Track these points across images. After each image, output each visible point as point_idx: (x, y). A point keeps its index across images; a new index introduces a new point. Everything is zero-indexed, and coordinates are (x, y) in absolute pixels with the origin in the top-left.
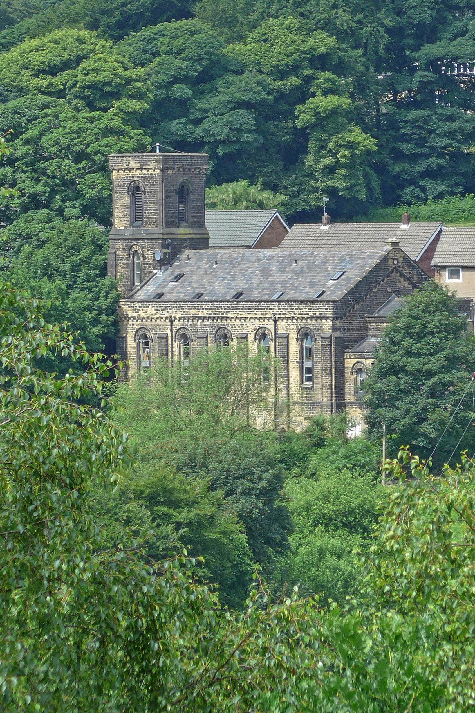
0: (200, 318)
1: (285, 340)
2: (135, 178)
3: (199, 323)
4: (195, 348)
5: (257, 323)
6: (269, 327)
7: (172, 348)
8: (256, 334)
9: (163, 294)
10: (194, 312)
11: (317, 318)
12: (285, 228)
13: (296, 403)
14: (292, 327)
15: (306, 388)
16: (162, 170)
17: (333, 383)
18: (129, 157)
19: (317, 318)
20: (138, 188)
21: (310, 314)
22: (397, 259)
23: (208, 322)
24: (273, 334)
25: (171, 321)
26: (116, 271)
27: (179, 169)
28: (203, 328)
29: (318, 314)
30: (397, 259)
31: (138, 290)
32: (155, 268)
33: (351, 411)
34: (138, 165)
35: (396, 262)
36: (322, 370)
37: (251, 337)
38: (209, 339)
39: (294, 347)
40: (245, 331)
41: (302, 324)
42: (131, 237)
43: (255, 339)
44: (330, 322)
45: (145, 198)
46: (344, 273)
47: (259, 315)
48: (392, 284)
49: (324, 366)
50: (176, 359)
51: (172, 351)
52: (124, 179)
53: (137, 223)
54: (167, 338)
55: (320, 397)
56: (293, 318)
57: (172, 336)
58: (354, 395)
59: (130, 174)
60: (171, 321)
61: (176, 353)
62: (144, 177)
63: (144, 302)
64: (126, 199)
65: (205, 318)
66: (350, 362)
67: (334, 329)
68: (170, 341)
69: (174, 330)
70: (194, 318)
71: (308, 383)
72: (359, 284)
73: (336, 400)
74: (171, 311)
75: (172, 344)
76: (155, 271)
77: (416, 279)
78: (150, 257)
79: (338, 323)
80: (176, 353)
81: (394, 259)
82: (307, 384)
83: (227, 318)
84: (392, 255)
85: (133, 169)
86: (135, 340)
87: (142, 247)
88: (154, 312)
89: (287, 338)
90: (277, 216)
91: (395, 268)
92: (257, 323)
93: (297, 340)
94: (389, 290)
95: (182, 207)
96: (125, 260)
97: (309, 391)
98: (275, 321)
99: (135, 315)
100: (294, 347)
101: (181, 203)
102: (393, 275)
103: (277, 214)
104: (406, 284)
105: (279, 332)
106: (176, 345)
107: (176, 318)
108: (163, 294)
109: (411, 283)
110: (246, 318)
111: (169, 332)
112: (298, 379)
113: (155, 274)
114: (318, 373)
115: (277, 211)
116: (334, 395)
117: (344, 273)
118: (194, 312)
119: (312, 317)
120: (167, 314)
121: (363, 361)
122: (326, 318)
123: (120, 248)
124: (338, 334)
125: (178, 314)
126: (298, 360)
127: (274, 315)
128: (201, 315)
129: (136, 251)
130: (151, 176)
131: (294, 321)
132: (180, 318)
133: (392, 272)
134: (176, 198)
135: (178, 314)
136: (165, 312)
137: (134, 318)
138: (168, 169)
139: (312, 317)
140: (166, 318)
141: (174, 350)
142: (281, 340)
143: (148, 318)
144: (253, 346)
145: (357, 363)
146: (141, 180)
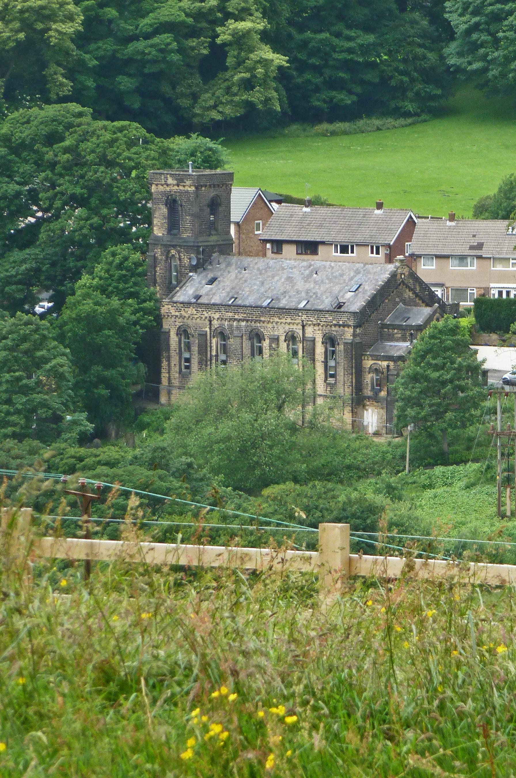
0: (235, 319)
1: (312, 343)
2: (173, 193)
3: (235, 323)
4: (231, 345)
5: (287, 327)
6: (298, 331)
7: (211, 343)
8: (286, 336)
9: (201, 296)
10: (230, 314)
11: (340, 326)
12: (266, 203)
13: (321, 395)
14: (318, 332)
15: (330, 384)
16: (197, 188)
17: (354, 381)
18: (167, 174)
19: (340, 326)
20: (175, 201)
21: (334, 322)
22: (404, 274)
23: (243, 324)
24: (301, 336)
25: (210, 321)
26: (156, 272)
27: (210, 186)
28: (238, 328)
29: (341, 323)
30: (404, 274)
31: (178, 291)
32: (190, 272)
33: (368, 403)
34: (175, 182)
35: (403, 277)
36: (344, 369)
37: (282, 338)
38: (244, 337)
39: (320, 349)
40: (276, 333)
41: (327, 330)
42: (169, 243)
43: (285, 341)
44: (351, 330)
45: (182, 209)
46: (360, 285)
47: (289, 320)
48: (400, 295)
49: (346, 366)
50: (214, 353)
51: (211, 347)
52: (164, 193)
53: (175, 231)
54: (206, 335)
55: (342, 391)
56: (319, 324)
57: (210, 334)
58: (371, 391)
59: (168, 189)
60: (210, 321)
61: (214, 348)
62: (181, 193)
63: (186, 303)
64: (164, 210)
65: (240, 320)
66: (368, 363)
67: (354, 335)
68: (208, 337)
69: (213, 328)
70: (231, 319)
71: (331, 379)
72: (374, 298)
73: (356, 395)
74: (210, 313)
75: (211, 340)
76: (191, 274)
77: (418, 289)
78: (186, 261)
79: (358, 330)
80: (214, 348)
81: (401, 274)
82: (331, 380)
83: (261, 321)
84: (399, 271)
85: (170, 185)
86: (177, 335)
87: (179, 252)
88: (195, 312)
89: (313, 341)
90: (260, 195)
91: (403, 281)
92: (287, 327)
93: (323, 343)
94: (397, 300)
95: (212, 218)
96: (163, 262)
97: (332, 386)
98: (303, 326)
99: (177, 314)
100: (320, 349)
101: (212, 214)
102: (400, 287)
103: (260, 191)
104: (411, 294)
105: (307, 335)
106: (214, 341)
107: (214, 319)
108: (201, 296)
109: (414, 293)
110: (277, 322)
111: (208, 329)
112: (323, 376)
113: (191, 276)
114: (341, 372)
115: (260, 189)
116: (354, 391)
117: (360, 285)
118: (230, 314)
119: (335, 325)
120: (206, 315)
121: (380, 362)
122: (349, 326)
123: (158, 252)
124: (358, 340)
125: (217, 316)
126: (323, 360)
127: (303, 321)
128: (236, 317)
129: (173, 255)
130: (187, 192)
131: (320, 327)
132: (218, 319)
133: (400, 285)
134: (208, 210)
135: (217, 316)
136: (204, 313)
137: (177, 316)
138: (202, 186)
139: (335, 325)
140: (206, 318)
141: (212, 345)
142: (308, 343)
143: (189, 317)
144: (283, 346)
145: (374, 364)
146: (178, 194)
